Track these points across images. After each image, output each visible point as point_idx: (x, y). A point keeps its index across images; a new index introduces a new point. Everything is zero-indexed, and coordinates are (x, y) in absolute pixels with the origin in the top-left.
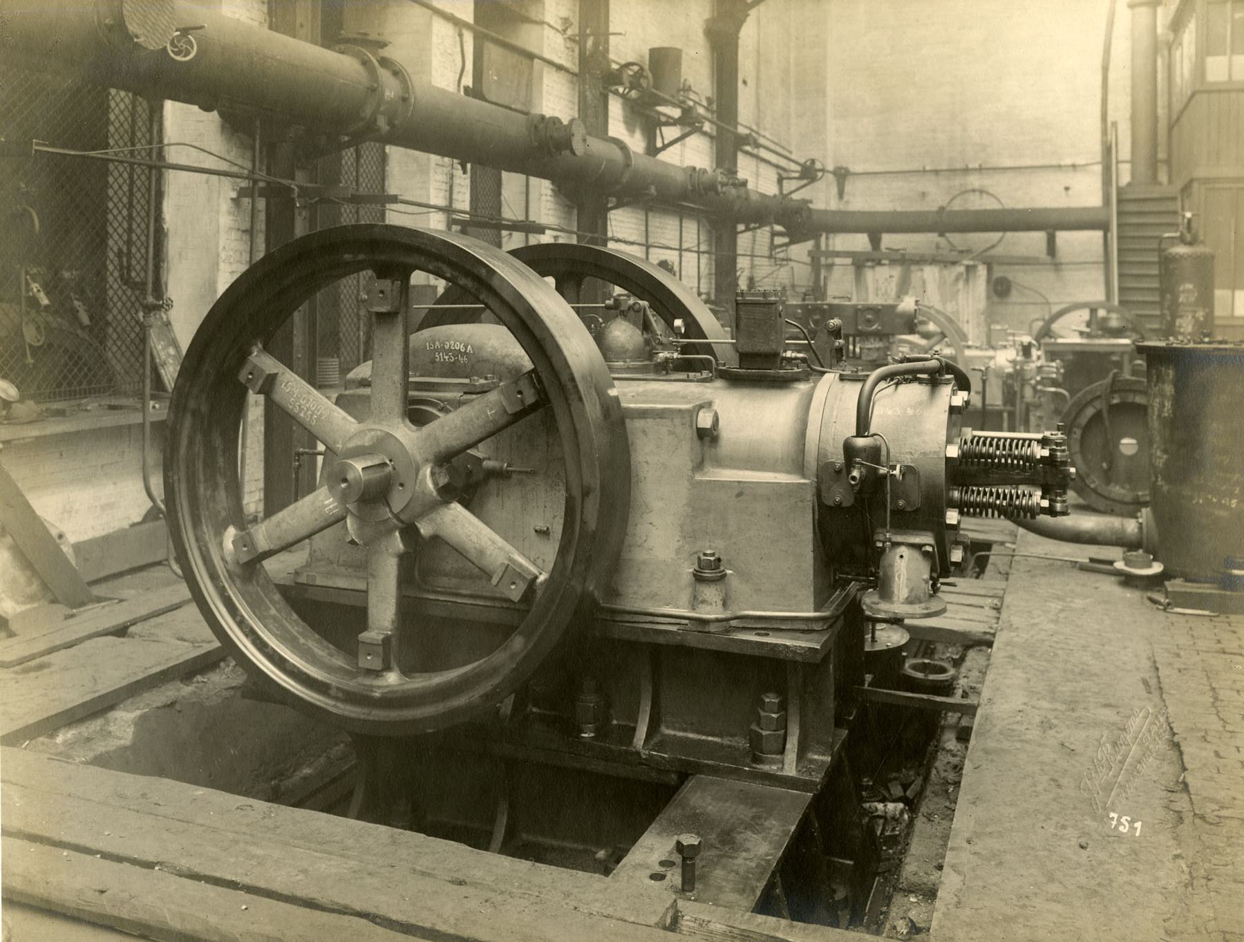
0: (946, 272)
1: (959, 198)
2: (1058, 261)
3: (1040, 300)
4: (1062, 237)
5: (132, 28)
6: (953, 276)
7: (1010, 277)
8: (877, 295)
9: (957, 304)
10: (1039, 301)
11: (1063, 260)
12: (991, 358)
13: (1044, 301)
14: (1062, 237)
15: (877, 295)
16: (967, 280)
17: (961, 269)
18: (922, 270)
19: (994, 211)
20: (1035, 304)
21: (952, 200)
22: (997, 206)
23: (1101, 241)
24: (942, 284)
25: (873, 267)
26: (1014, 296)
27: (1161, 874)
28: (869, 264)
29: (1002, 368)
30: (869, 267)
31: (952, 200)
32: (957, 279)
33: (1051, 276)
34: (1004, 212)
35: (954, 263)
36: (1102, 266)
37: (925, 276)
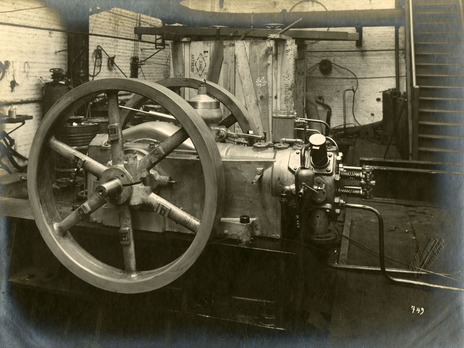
0: (255, 47)
1: (298, 6)
2: (363, 49)
3: (351, 76)
4: (366, 30)
5: (319, 62)
6: (263, 52)
7: (331, 60)
8: (193, 70)
9: (266, 79)
10: (350, 77)
11: (368, 49)
12: (268, 164)
13: (353, 76)
14: (366, 30)
15: (193, 70)
16: (276, 56)
17: (271, 44)
18: (234, 45)
19: (321, 12)
20: (348, 78)
21: (294, 7)
22: (323, 9)
23: (393, 35)
24: (252, 59)
25: (189, 42)
26: (334, 73)
27: (363, 65)
28: (185, 39)
29: (281, 181)
30: (185, 42)
31: (294, 7)
32: (267, 54)
33: (358, 59)
34: (327, 14)
35: (265, 38)
36: (394, 52)
37: (237, 52)
